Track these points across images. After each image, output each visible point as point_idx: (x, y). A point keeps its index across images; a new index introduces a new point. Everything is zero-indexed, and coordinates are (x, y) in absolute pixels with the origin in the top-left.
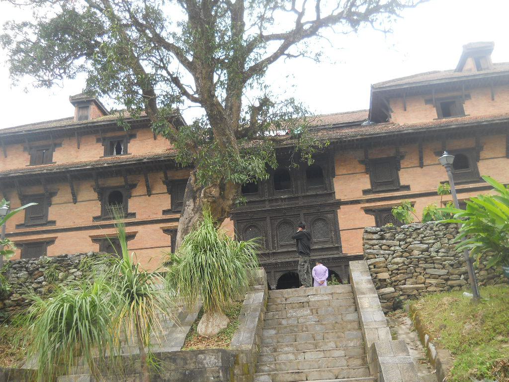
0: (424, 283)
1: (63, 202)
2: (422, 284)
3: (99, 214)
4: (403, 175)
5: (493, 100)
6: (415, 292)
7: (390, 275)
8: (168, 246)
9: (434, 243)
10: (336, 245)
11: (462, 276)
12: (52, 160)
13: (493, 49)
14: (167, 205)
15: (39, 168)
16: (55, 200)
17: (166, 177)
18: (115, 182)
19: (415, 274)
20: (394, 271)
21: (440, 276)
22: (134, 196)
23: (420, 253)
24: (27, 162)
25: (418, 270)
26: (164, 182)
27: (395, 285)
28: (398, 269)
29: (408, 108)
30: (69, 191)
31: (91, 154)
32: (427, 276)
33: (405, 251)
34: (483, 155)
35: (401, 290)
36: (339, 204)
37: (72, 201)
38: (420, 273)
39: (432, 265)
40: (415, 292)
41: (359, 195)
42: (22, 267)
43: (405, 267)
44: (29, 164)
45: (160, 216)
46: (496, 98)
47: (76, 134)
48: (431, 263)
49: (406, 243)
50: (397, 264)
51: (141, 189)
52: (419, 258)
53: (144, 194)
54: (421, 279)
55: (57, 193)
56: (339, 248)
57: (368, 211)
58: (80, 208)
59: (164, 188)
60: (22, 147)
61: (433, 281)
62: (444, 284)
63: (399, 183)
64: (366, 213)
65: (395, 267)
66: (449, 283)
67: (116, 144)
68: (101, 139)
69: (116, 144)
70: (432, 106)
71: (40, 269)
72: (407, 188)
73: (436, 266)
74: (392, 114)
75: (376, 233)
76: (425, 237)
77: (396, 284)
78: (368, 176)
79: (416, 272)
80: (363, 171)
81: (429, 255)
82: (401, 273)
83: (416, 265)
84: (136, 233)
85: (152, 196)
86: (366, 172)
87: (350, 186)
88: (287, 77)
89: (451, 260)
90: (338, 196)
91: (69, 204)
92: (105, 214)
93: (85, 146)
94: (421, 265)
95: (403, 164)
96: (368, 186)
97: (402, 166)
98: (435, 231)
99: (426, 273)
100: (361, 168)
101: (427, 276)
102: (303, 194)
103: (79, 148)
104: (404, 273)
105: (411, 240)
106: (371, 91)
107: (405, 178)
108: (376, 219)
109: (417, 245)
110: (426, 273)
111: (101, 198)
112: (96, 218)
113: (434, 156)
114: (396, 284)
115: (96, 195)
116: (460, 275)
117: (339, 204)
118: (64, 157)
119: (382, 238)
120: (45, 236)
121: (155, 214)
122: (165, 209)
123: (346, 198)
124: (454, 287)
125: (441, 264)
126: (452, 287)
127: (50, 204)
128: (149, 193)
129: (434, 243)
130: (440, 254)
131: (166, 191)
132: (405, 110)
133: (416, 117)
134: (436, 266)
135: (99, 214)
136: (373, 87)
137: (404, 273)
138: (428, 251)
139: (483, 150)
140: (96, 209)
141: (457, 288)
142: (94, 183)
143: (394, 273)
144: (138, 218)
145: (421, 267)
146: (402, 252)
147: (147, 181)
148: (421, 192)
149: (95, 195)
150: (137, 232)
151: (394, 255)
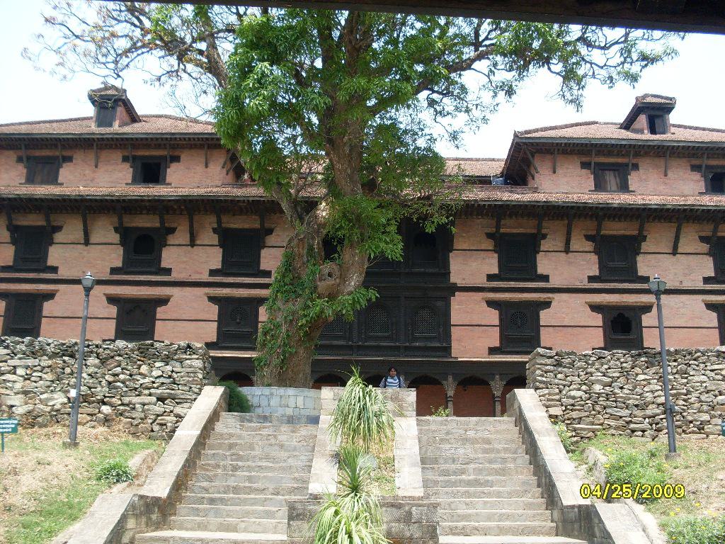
0: (601, 424)
1: (70, 242)
2: (599, 425)
3: (119, 264)
4: (542, 260)
5: (666, 175)
6: (591, 434)
7: (564, 411)
8: (158, 320)
9: (618, 378)
10: (444, 345)
11: (647, 420)
12: (57, 180)
13: (673, 108)
14: (217, 263)
15: (42, 190)
16: (59, 237)
17: (219, 222)
18: (147, 222)
19: (593, 412)
20: (568, 407)
21: (621, 417)
22: (169, 245)
23: (602, 387)
24: (21, 179)
25: (598, 408)
26: (215, 231)
27: (567, 424)
28: (573, 405)
29: (559, 171)
30: (81, 226)
31: (112, 180)
32: (607, 416)
33: (585, 384)
34: (645, 247)
35: (575, 430)
36: (455, 289)
37: (83, 242)
38: (599, 413)
39: (614, 404)
40: (591, 434)
41: (481, 281)
42: (92, 352)
43: (583, 403)
44: (24, 181)
45: (205, 277)
46: (670, 174)
47: (95, 145)
48: (613, 401)
49: (586, 374)
50: (574, 398)
51: (181, 236)
52: (598, 394)
53: (560, 250)
54: (600, 420)
55: (62, 227)
56: (447, 350)
57: (491, 303)
58: (94, 252)
59: (215, 239)
60: (15, 156)
61: (613, 423)
62: (625, 427)
63: (536, 271)
64: (488, 306)
65: (571, 401)
66: (632, 426)
67: (151, 172)
68: (131, 159)
69: (151, 172)
70: (589, 171)
71: (117, 358)
72: (545, 278)
73: (619, 404)
74: (536, 176)
75: (551, 357)
76: (609, 368)
77: (569, 422)
78: (496, 255)
79: (594, 410)
80: (592, 250)
81: (611, 391)
82: (575, 410)
83: (595, 402)
84: (57, 291)
85: (195, 247)
86: (495, 251)
87: (472, 265)
88: (458, 147)
89: (637, 399)
90: (455, 278)
91: (79, 246)
92: (228, 268)
93: (106, 165)
94: (601, 403)
95: (545, 245)
96: (495, 270)
97: (542, 248)
98: (622, 363)
99: (606, 413)
100: (489, 244)
101: (607, 416)
102: (407, 270)
103: (96, 167)
104: (579, 410)
105: (593, 370)
106: (513, 140)
107: (544, 264)
108: (500, 315)
109: (599, 378)
110: (606, 413)
111: (123, 242)
112: (114, 271)
113: (584, 240)
114: (569, 422)
115: (118, 236)
116: (645, 419)
117: (455, 289)
118: (77, 180)
119: (559, 364)
120: (43, 287)
121: (198, 273)
122: (214, 267)
123: (464, 282)
124: (636, 431)
125: (624, 403)
126: (633, 431)
127: (51, 243)
128: (192, 244)
129: (618, 378)
130: (626, 391)
131: (216, 242)
132: (554, 172)
133: (564, 186)
134: (619, 404)
135: (119, 264)
136: (516, 135)
137: (579, 410)
138: (610, 386)
139: (645, 241)
140: (116, 257)
141: (640, 433)
142: (116, 219)
143: (568, 409)
144: (175, 276)
145: (601, 405)
146: (580, 384)
147: (191, 226)
148: (560, 287)
149: (116, 238)
150: (172, 296)
151: (571, 387)
